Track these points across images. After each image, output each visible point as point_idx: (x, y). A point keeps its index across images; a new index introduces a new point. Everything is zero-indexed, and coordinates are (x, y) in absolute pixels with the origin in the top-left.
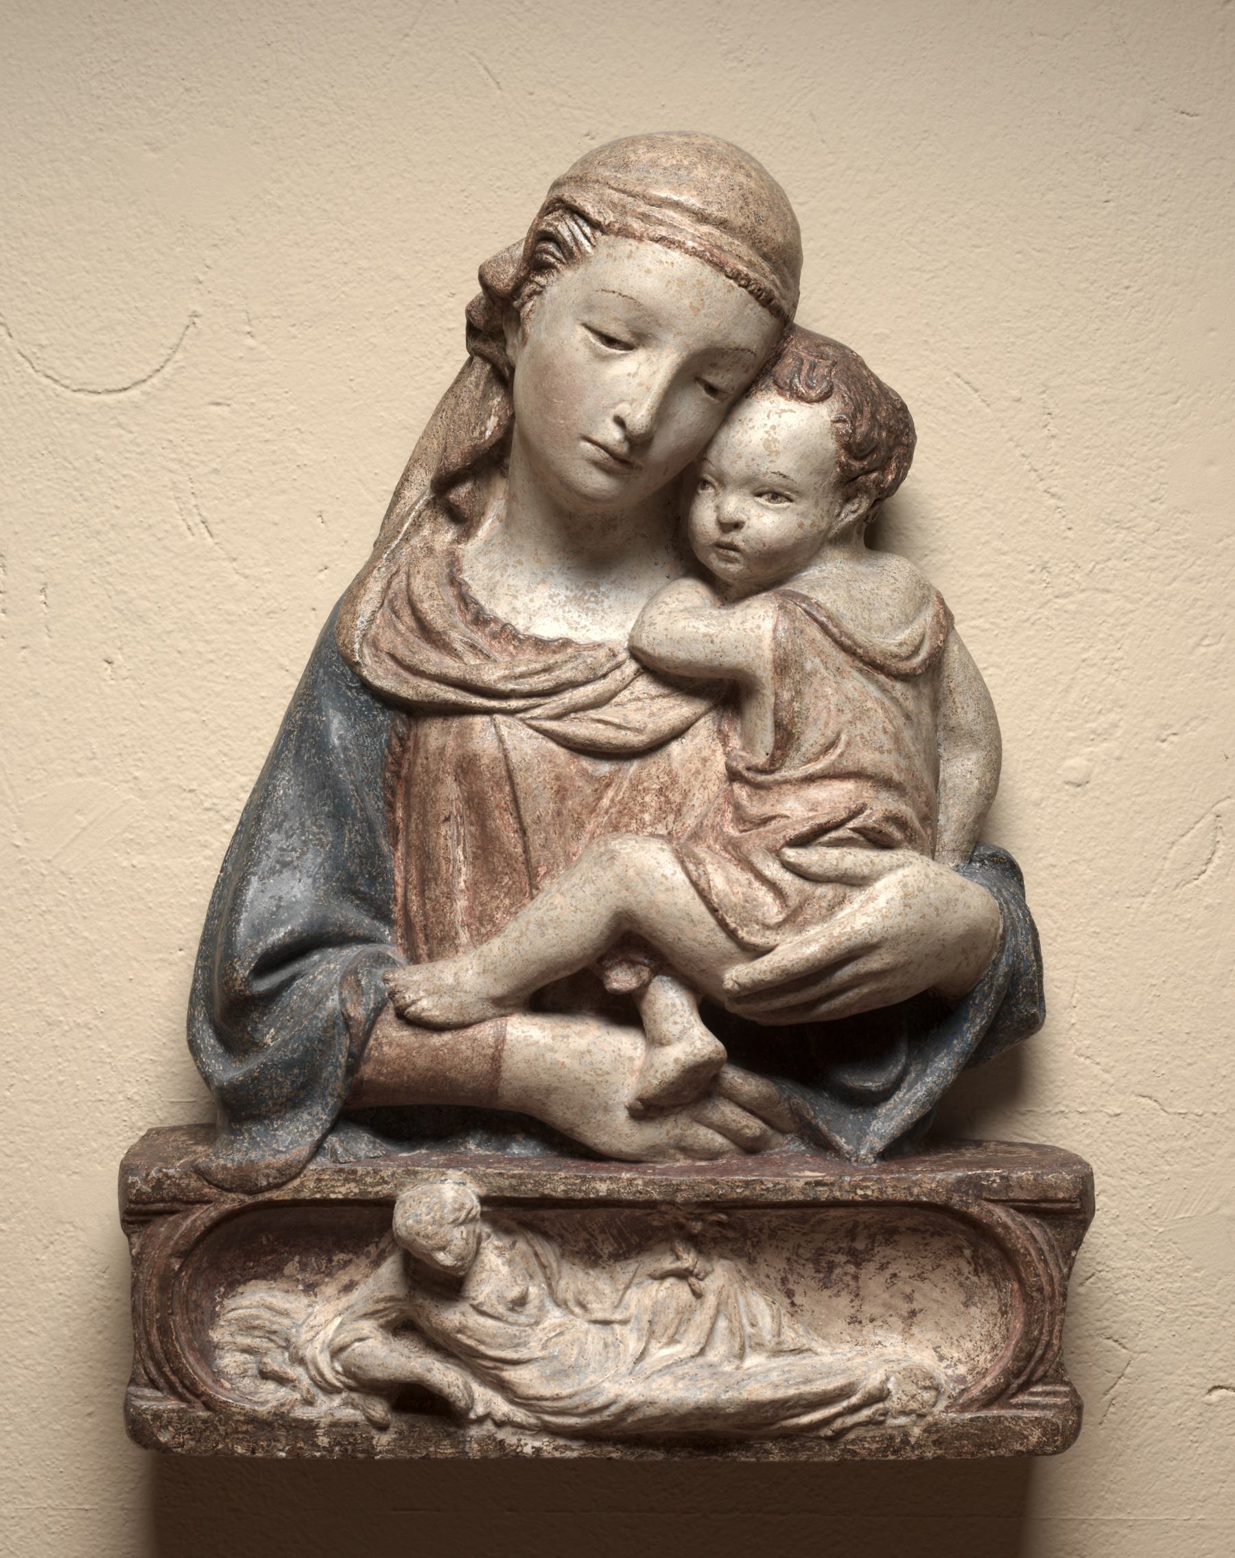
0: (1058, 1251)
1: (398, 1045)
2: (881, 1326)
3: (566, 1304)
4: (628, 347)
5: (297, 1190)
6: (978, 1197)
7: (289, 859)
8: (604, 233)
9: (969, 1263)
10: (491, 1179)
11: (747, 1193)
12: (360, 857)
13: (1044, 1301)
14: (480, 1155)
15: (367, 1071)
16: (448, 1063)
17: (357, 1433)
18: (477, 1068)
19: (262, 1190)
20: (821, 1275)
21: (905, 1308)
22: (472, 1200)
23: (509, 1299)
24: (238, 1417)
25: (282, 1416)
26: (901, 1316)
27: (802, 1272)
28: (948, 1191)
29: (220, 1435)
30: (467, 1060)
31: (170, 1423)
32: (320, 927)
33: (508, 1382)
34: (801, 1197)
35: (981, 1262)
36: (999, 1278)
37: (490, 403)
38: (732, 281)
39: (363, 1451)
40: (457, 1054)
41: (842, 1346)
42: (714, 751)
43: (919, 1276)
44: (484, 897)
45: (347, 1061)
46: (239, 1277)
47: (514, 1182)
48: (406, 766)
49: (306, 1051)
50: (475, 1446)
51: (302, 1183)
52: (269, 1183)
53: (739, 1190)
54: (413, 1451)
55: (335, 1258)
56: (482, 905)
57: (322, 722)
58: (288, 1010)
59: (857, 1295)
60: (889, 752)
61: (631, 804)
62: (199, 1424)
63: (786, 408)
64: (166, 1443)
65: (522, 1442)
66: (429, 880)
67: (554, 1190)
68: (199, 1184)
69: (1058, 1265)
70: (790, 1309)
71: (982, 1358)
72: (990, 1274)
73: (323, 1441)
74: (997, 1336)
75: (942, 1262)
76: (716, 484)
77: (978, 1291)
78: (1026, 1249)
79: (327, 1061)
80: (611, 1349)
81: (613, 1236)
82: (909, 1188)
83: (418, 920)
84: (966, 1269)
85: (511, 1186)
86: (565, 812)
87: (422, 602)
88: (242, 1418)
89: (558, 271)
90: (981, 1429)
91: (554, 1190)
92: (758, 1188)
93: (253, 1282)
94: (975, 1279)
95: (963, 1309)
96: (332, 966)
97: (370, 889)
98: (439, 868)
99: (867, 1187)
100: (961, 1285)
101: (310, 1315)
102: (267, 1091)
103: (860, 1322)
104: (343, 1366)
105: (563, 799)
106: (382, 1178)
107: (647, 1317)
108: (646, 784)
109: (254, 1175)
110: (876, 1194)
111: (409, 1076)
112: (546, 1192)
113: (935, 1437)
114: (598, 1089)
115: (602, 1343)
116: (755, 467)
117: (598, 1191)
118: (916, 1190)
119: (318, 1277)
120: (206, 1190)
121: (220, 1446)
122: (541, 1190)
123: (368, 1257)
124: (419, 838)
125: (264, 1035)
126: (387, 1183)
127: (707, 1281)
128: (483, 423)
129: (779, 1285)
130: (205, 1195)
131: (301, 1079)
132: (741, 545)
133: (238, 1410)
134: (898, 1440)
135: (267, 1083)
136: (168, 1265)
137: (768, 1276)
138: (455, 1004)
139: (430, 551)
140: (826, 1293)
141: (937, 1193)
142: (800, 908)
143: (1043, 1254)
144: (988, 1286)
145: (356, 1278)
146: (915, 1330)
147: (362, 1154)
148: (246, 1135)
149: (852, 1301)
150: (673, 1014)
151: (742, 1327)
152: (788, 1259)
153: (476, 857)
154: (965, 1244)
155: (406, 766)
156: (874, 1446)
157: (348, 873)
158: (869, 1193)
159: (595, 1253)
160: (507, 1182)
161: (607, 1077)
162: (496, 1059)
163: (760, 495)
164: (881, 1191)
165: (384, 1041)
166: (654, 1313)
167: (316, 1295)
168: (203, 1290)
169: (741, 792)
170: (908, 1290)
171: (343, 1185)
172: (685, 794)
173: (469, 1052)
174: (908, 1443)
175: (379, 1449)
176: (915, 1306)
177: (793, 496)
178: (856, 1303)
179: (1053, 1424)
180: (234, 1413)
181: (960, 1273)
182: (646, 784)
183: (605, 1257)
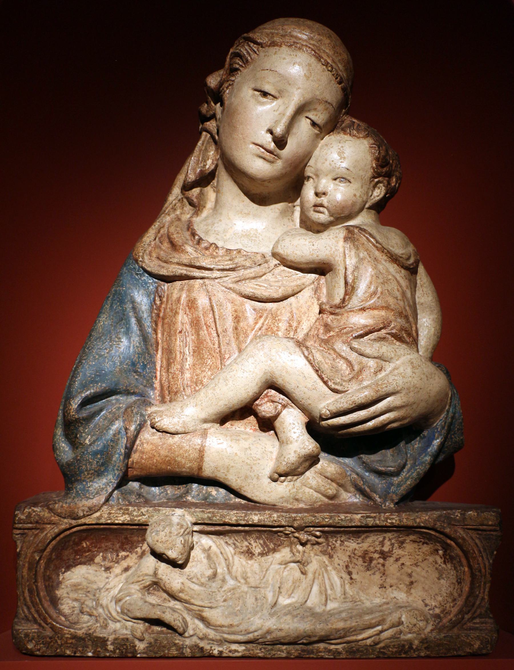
0: (488, 551)
1: (152, 444)
2: (396, 589)
3: (236, 578)
4: (275, 97)
5: (99, 518)
6: (449, 524)
7: (103, 353)
8: (262, 47)
9: (441, 558)
10: (198, 514)
11: (331, 521)
12: (138, 354)
13: (481, 577)
14: (193, 502)
15: (135, 457)
16: (177, 453)
17: (128, 644)
18: (192, 456)
19: (80, 518)
20: (366, 564)
21: (407, 580)
22: (187, 524)
23: (207, 575)
24: (67, 636)
25: (90, 635)
26: (405, 584)
27: (356, 562)
28: (434, 521)
29: (58, 645)
30: (186, 451)
31: (33, 639)
32: (116, 385)
33: (206, 618)
34: (359, 524)
35: (448, 557)
36: (457, 565)
37: (209, 153)
38: (325, 67)
39: (130, 653)
40: (181, 448)
41: (376, 599)
42: (313, 303)
43: (415, 564)
44: (198, 371)
45: (125, 451)
46: (72, 563)
47: (210, 515)
48: (163, 311)
49: (104, 446)
50: (188, 650)
51: (101, 515)
52: (84, 515)
53: (327, 520)
54: (157, 653)
55: (120, 554)
56: (197, 376)
57: (123, 290)
58: (98, 426)
59: (384, 574)
60: (400, 300)
61: (272, 326)
62: (48, 640)
63: (348, 139)
64: (31, 649)
65: (213, 648)
66: (171, 363)
67: (231, 519)
68: (49, 515)
69: (488, 559)
70: (350, 581)
71: (448, 605)
72: (452, 563)
73: (111, 647)
74: (456, 594)
75: (427, 558)
76: (314, 177)
77: (445, 572)
78: (474, 551)
79: (115, 452)
80: (259, 601)
81: (260, 544)
82: (414, 519)
83: (166, 384)
84: (440, 561)
85: (208, 517)
86: (239, 328)
87: (173, 235)
88: (69, 636)
89: (241, 71)
90: (450, 642)
91: (231, 519)
92: (337, 519)
93: (79, 566)
94: (444, 566)
95: (437, 581)
96: (121, 405)
97: (143, 371)
98: (176, 356)
99: (393, 519)
100: (437, 569)
101: (106, 583)
102: (84, 467)
103: (385, 587)
104: (121, 609)
105: (238, 322)
106: (142, 512)
107: (278, 585)
108: (279, 317)
109: (76, 510)
110: (398, 522)
111: (157, 460)
112: (226, 520)
113: (426, 645)
114: (254, 468)
115: (254, 598)
116: (333, 165)
117: (253, 520)
118: (418, 520)
119: (111, 564)
120: (53, 518)
121: (58, 650)
122: (224, 519)
123: (137, 554)
124: (167, 344)
125: (85, 440)
126: (144, 515)
127: (308, 566)
128: (205, 161)
129: (345, 569)
130: (52, 521)
131: (102, 461)
132: (326, 204)
133: (67, 632)
134: (407, 647)
135: (84, 463)
136: (32, 556)
137: (339, 565)
138: (181, 422)
139: (179, 219)
140: (369, 573)
141: (429, 521)
142: (361, 371)
143: (481, 553)
144: (451, 569)
145: (131, 564)
146: (413, 591)
147: (132, 500)
148: (75, 490)
149: (381, 577)
150: (293, 428)
151: (326, 590)
152: (350, 556)
153: (194, 352)
154: (440, 548)
155: (163, 311)
156: (395, 650)
157: (132, 362)
158: (394, 521)
159: (251, 553)
160: (206, 516)
161: (258, 461)
162: (201, 452)
163: (335, 179)
164: (400, 520)
165: (145, 441)
166: (281, 583)
167: (110, 573)
168: (53, 570)
169: (329, 319)
170: (409, 571)
171: (122, 516)
172: (299, 323)
173: (187, 447)
174: (412, 648)
175: (139, 651)
176: (413, 579)
177: (352, 180)
178: (384, 578)
179: (486, 639)
180: (65, 634)
181: (436, 563)
182: (279, 317)
183: (256, 555)
